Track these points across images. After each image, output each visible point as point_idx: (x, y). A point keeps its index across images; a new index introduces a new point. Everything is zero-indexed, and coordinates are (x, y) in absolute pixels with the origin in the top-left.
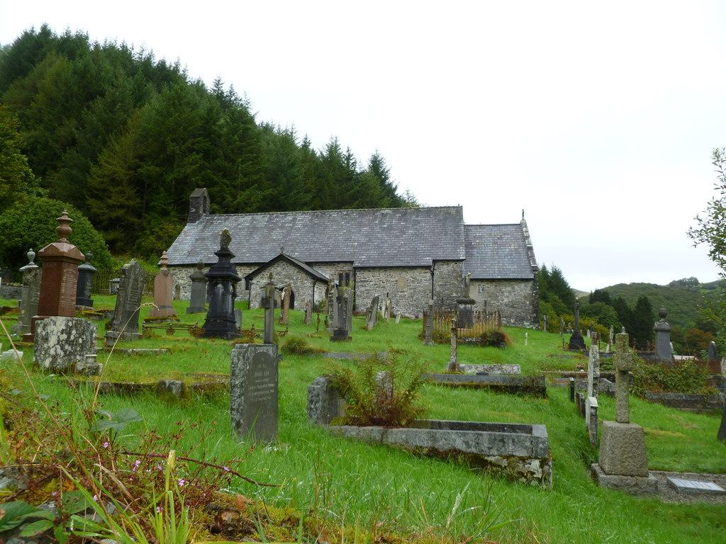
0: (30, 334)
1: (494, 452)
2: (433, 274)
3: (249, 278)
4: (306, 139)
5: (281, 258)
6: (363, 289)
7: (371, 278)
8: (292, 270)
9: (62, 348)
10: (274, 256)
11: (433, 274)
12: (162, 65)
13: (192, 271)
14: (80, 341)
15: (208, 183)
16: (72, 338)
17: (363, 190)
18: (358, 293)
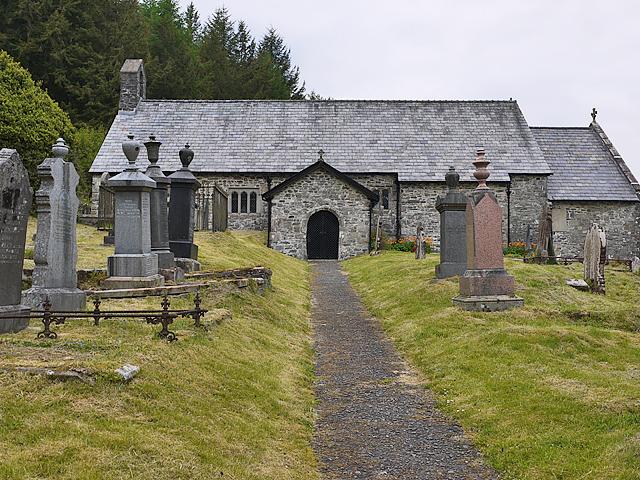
2: (509, 193)
3: (268, 197)
4: (192, 7)
5: (321, 167)
6: (412, 212)
7: (423, 197)
8: (336, 186)
10: (308, 163)
11: (509, 193)
13: (441, 193)
17: (256, 74)
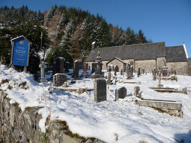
0: (187, 57)
1: (164, 108)
2: (156, 61)
9: (59, 81)
11: (156, 61)
12: (84, 12)
14: (63, 80)
15: (8, 53)
16: (61, 79)
18: (136, 67)
